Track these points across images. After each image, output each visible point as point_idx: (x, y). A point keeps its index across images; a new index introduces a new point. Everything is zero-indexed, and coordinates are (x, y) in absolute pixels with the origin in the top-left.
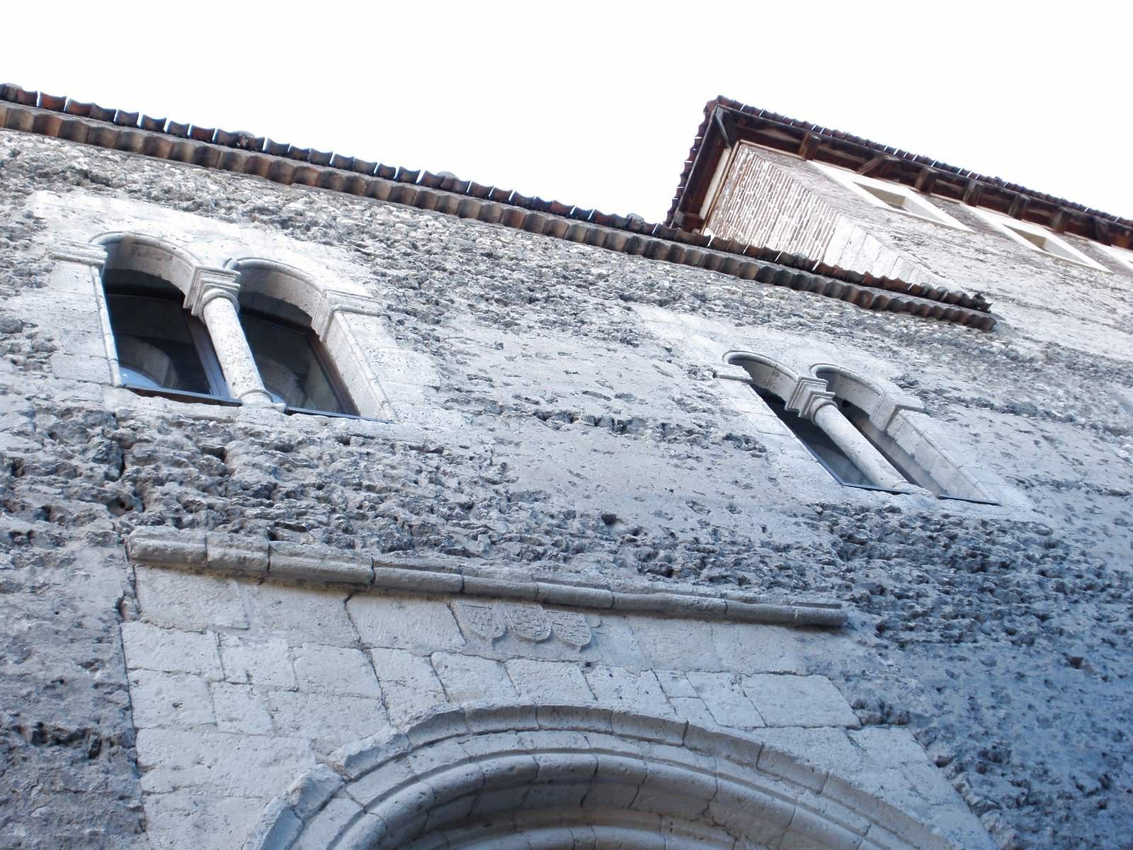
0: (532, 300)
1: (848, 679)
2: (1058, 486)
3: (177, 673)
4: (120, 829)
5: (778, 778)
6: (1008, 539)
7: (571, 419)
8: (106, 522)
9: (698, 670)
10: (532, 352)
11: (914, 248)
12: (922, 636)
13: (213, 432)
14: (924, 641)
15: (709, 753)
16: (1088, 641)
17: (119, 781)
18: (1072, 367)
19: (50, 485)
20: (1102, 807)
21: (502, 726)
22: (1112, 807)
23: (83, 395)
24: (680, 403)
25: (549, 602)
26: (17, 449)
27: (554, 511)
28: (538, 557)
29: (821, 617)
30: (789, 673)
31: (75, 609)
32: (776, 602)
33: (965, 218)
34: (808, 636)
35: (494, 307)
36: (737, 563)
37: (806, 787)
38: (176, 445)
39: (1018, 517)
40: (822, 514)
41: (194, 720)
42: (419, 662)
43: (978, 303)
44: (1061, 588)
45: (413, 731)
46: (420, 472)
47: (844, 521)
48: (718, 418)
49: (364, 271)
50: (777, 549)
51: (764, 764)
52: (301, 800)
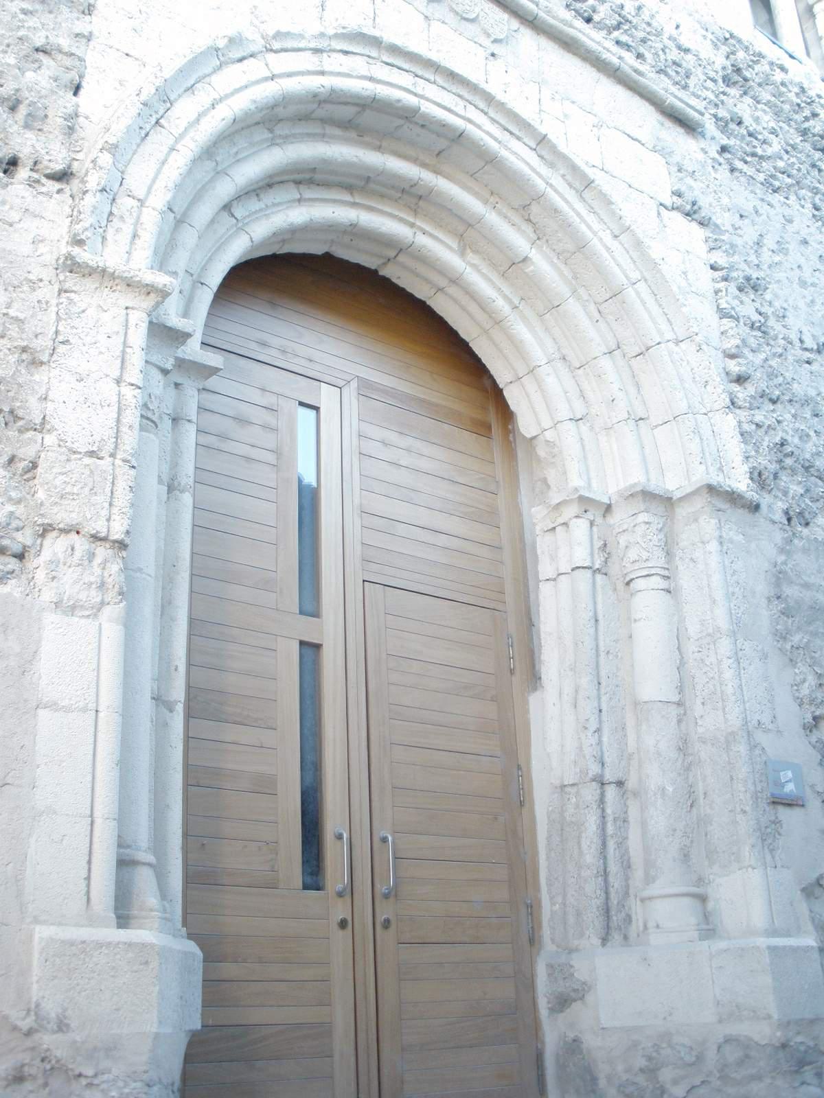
1: (679, 171)
5: (592, 210)
15: (552, 165)
20: (808, 362)
30: (639, 142)
34: (668, 123)
37: (608, 228)
47: (741, 55)
50: (679, 47)
51: (586, 194)
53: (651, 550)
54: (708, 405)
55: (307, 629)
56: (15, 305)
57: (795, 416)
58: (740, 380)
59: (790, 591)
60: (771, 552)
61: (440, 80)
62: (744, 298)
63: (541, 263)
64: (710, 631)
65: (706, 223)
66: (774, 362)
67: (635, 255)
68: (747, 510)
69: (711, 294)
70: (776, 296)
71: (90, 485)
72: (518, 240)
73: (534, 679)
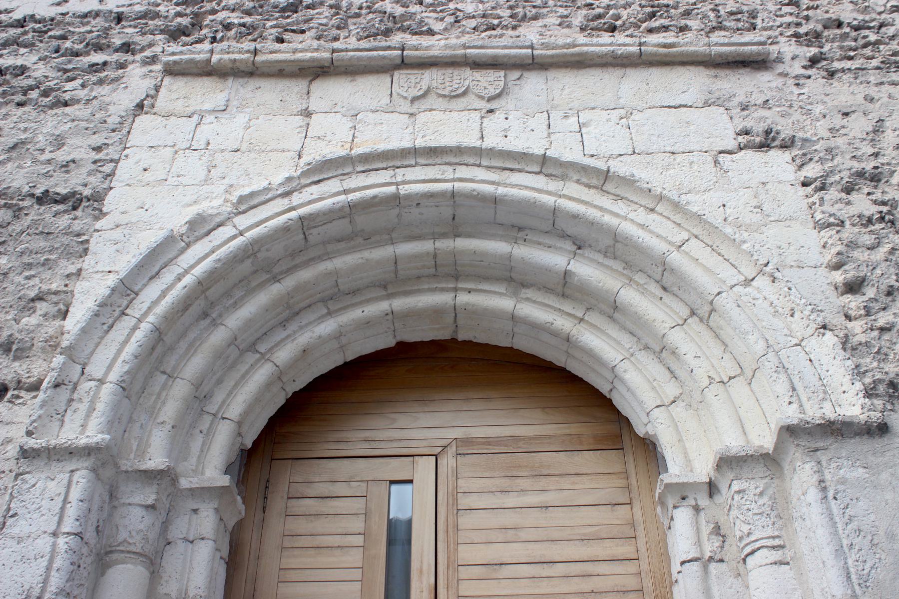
9: (593, 108)
14: (856, 69)
15: (563, 178)
21: (380, 165)
25: (478, 64)
29: (739, 54)
30: (685, 106)
32: (696, 45)
34: (722, 73)
37: (641, 206)
51: (609, 187)
53: (751, 521)
54: (798, 334)
61: (422, 161)
63: (587, 271)
65: (789, 144)
67: (677, 218)
68: (866, 436)
72: (554, 259)
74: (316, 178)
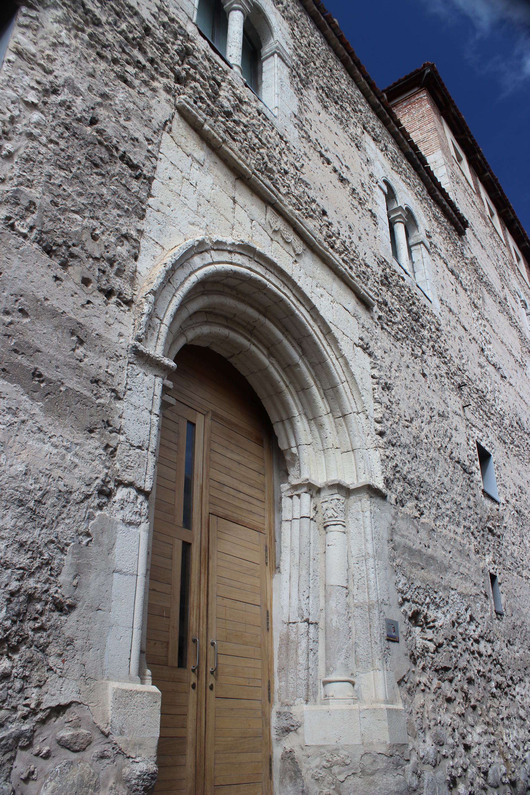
0: (336, 103)
1: (363, 327)
2: (450, 310)
3: (175, 166)
4: (136, 213)
5: (329, 345)
6: (428, 317)
7: (329, 162)
8: (172, 83)
10: (327, 125)
11: (455, 182)
12: (389, 330)
13: (220, 73)
15: (315, 320)
16: (431, 371)
17: (143, 194)
18: (476, 270)
19: (157, 50)
20: (407, 427)
22: (410, 429)
23: (180, 17)
24: (362, 184)
26: (150, 22)
27: (311, 196)
28: (299, 210)
31: (151, 113)
33: (476, 185)
35: (324, 95)
36: (353, 260)
38: (205, 68)
39: (435, 312)
40: (382, 262)
41: (174, 189)
42: (244, 223)
43: (465, 224)
44: (433, 347)
45: (239, 245)
46: (277, 146)
47: (388, 270)
48: (370, 200)
49: (291, 42)
50: (365, 264)
52: (198, 245)
55: (185, 535)
56: (110, 368)
57: (401, 453)
58: (381, 434)
59: (397, 538)
60: (390, 518)
62: (384, 393)
64: (364, 554)
66: (394, 426)
67: (344, 369)
69: (371, 390)
70: (396, 393)
71: (138, 463)
73: (276, 568)
74: (243, 252)
